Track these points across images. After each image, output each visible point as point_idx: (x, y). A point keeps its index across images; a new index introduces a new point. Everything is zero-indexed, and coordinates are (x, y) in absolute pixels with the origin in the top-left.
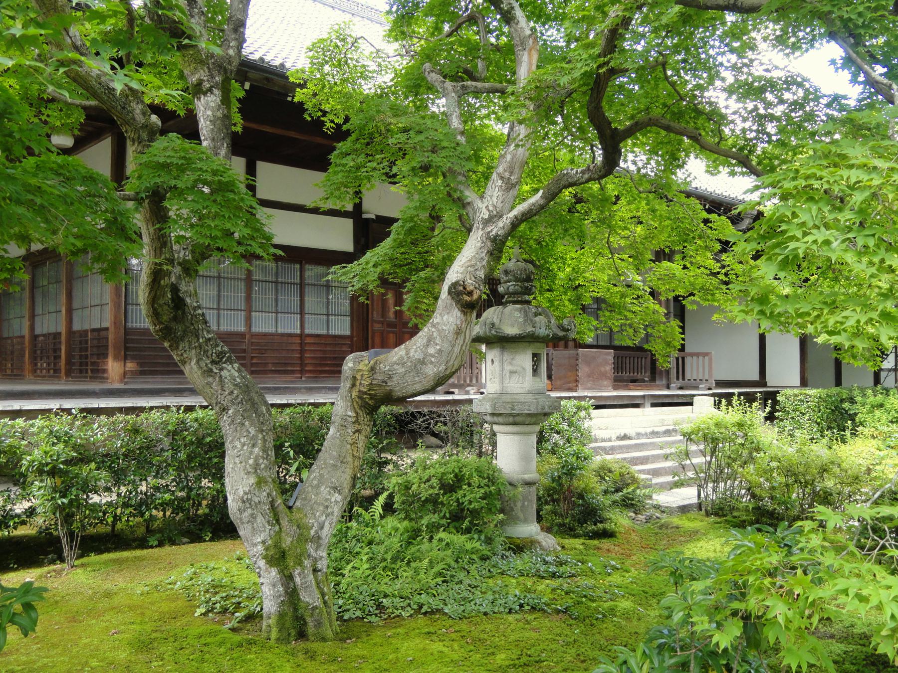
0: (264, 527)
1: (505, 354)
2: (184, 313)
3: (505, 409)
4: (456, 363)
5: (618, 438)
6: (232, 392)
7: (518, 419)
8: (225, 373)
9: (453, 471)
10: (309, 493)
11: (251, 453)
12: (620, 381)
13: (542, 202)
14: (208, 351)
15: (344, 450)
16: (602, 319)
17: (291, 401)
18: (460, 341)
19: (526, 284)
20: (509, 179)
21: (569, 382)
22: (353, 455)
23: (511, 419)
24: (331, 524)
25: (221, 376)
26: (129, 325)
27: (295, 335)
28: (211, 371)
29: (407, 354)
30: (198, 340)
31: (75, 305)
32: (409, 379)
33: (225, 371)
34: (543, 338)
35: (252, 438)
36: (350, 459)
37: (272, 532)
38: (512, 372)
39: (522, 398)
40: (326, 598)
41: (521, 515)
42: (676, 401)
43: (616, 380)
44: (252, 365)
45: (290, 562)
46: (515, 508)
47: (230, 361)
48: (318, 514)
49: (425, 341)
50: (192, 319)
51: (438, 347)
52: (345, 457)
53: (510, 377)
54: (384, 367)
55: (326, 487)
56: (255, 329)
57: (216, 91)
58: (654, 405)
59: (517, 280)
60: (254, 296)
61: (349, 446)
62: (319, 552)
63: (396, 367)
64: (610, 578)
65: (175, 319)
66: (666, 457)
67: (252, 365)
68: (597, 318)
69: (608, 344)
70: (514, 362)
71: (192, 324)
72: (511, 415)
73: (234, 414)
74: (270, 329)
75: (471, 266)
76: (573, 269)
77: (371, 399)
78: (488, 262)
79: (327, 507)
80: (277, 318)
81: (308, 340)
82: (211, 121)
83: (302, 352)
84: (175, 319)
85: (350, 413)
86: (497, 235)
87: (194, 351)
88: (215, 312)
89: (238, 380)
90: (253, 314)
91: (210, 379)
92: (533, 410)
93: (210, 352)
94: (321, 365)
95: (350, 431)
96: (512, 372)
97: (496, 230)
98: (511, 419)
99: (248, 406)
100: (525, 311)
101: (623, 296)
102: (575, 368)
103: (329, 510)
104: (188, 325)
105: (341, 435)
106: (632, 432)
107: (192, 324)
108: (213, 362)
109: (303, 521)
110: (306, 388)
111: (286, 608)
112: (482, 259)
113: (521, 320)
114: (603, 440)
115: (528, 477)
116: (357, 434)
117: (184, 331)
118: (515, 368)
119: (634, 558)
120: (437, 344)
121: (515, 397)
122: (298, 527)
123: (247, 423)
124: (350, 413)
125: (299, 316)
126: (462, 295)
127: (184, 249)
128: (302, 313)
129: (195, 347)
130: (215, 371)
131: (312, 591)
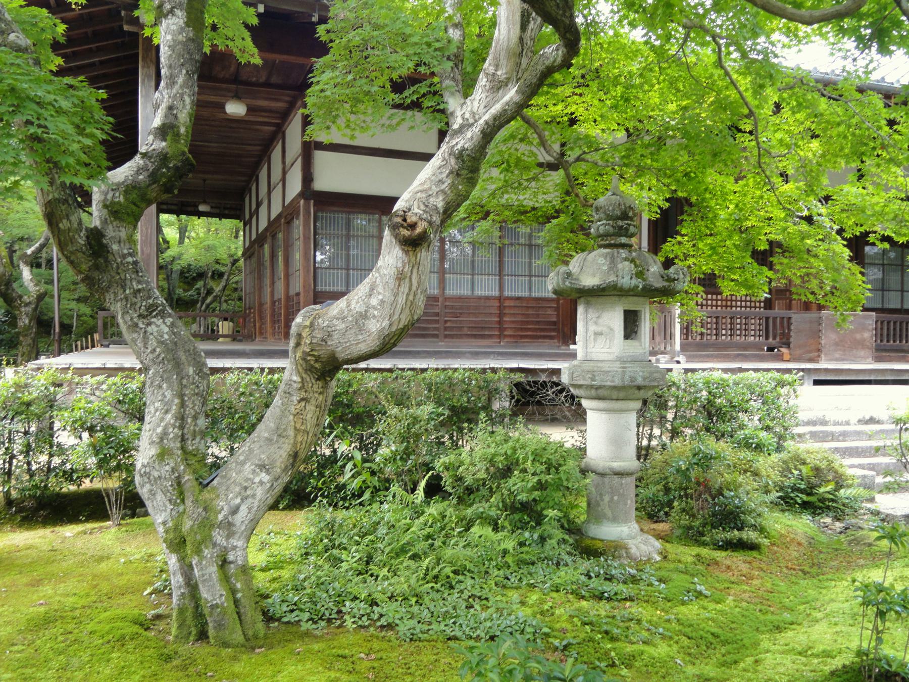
0: (166, 506)
1: (590, 310)
2: (107, 260)
3: (584, 379)
4: (403, 317)
5: (859, 421)
6: (154, 350)
7: (601, 392)
8: (152, 329)
9: (506, 453)
10: (231, 469)
11: (162, 420)
12: (886, 350)
13: (517, 98)
14: (135, 304)
15: (285, 421)
16: (778, 267)
17: (228, 365)
18: (404, 289)
19: (620, 223)
20: (494, 74)
21: (810, 352)
22: (295, 428)
23: (593, 392)
24: (250, 509)
25: (145, 332)
26: (319, 288)
27: (494, 298)
28: (136, 325)
29: (348, 305)
30: (125, 291)
31: (291, 271)
32: (350, 335)
33: (153, 326)
34: (630, 290)
35: (166, 404)
36: (291, 433)
37: (174, 513)
38: (597, 334)
39: (606, 367)
40: (239, 595)
41: (609, 513)
42: (872, 378)
43: (878, 349)
44: (446, 329)
45: (189, 549)
46: (601, 503)
47: (162, 315)
48: (231, 495)
49: (367, 290)
50: (118, 268)
51: (380, 297)
52: (285, 430)
53: (595, 340)
54: (322, 322)
55: (252, 464)
56: (449, 292)
57: (178, 12)
58: (817, 383)
59: (609, 217)
60: (506, 259)
61: (291, 417)
62: (231, 541)
63: (335, 322)
64: (683, 609)
65: (96, 267)
66: (877, 451)
67: (446, 329)
68: (771, 268)
69: (899, 307)
70: (600, 321)
71: (119, 274)
72: (591, 387)
73: (154, 374)
74: (466, 292)
75: (421, 191)
76: (737, 206)
77: (316, 361)
78: (453, 186)
79: (246, 488)
80: (348, 276)
81: (507, 303)
82: (169, 47)
83: (501, 315)
84: (96, 267)
85: (295, 378)
86: (463, 149)
87: (119, 304)
88: (344, 272)
89: (166, 337)
90: (447, 276)
91: (135, 335)
92: (617, 382)
93: (139, 305)
94: (522, 329)
95: (295, 399)
96: (597, 334)
97: (462, 142)
98: (593, 392)
99: (170, 367)
100: (613, 257)
101: (803, 236)
102: (816, 334)
103: (249, 492)
104: (113, 274)
105: (282, 404)
106: (831, 416)
107: (119, 274)
108: (141, 316)
109: (214, 503)
110: (469, 352)
111: (187, 602)
112: (441, 181)
113: (605, 268)
114: (836, 423)
115: (617, 465)
116: (303, 404)
117: (110, 282)
118: (599, 329)
119: (755, 582)
120: (379, 293)
121: (600, 364)
122: (205, 509)
123: (165, 386)
124: (295, 378)
125: (497, 278)
126: (398, 228)
127: (113, 190)
128: (501, 274)
129: (121, 299)
130: (141, 325)
131: (213, 586)
